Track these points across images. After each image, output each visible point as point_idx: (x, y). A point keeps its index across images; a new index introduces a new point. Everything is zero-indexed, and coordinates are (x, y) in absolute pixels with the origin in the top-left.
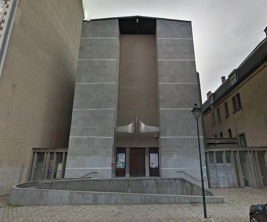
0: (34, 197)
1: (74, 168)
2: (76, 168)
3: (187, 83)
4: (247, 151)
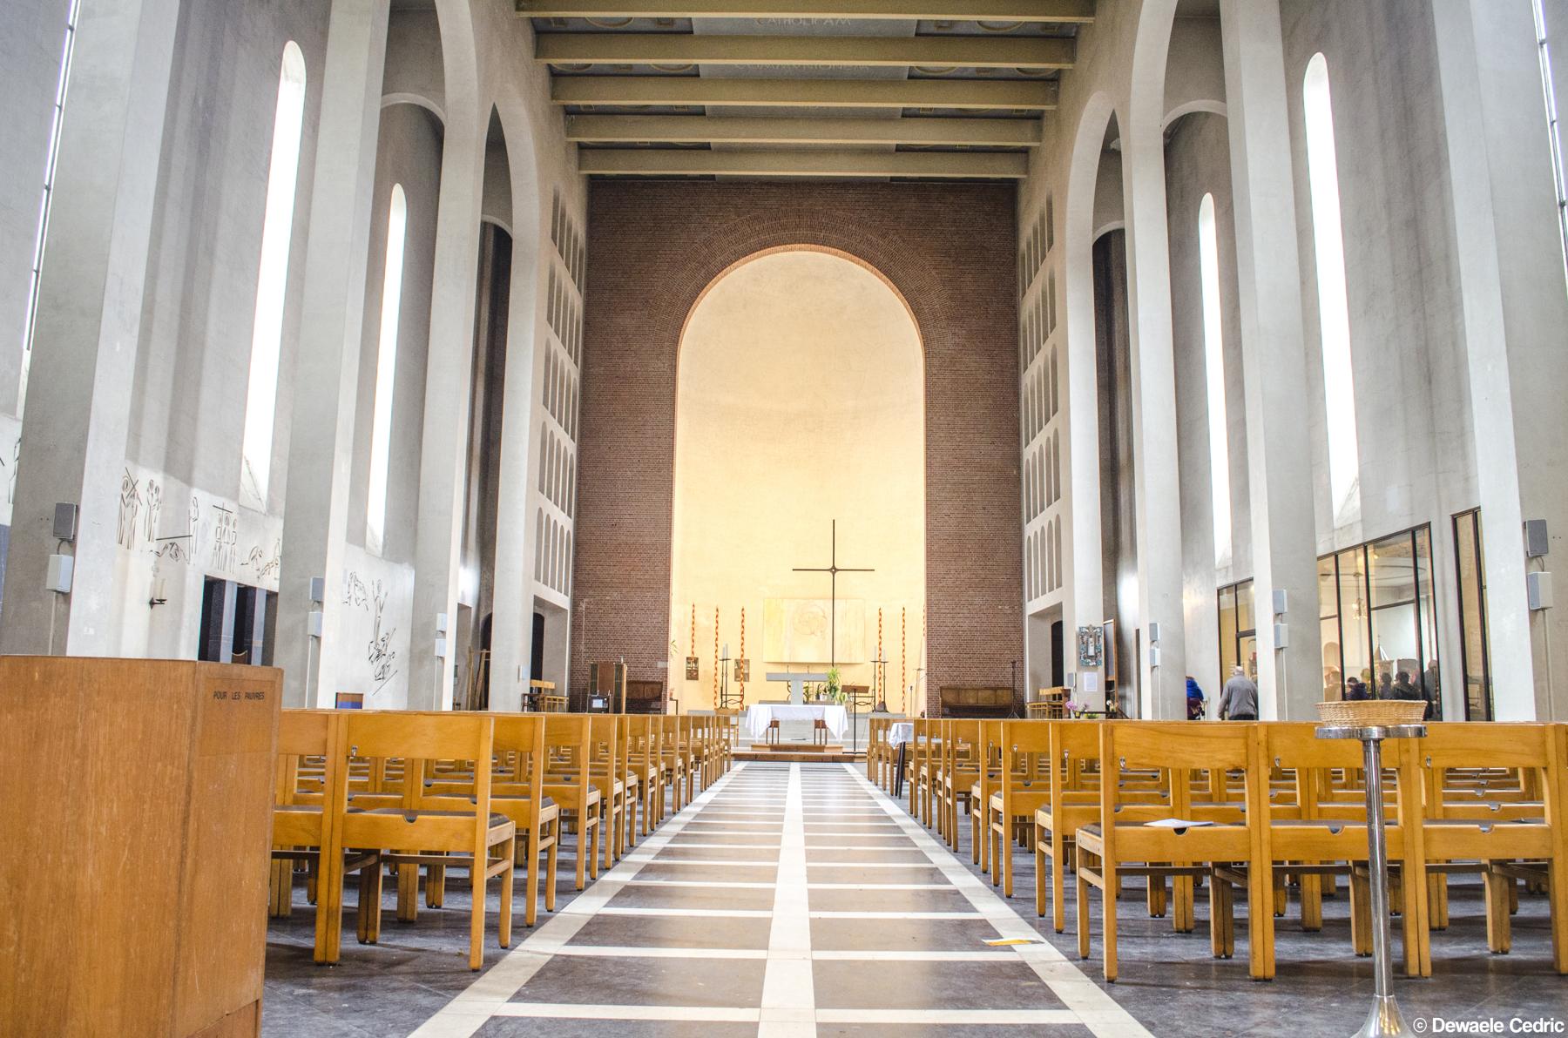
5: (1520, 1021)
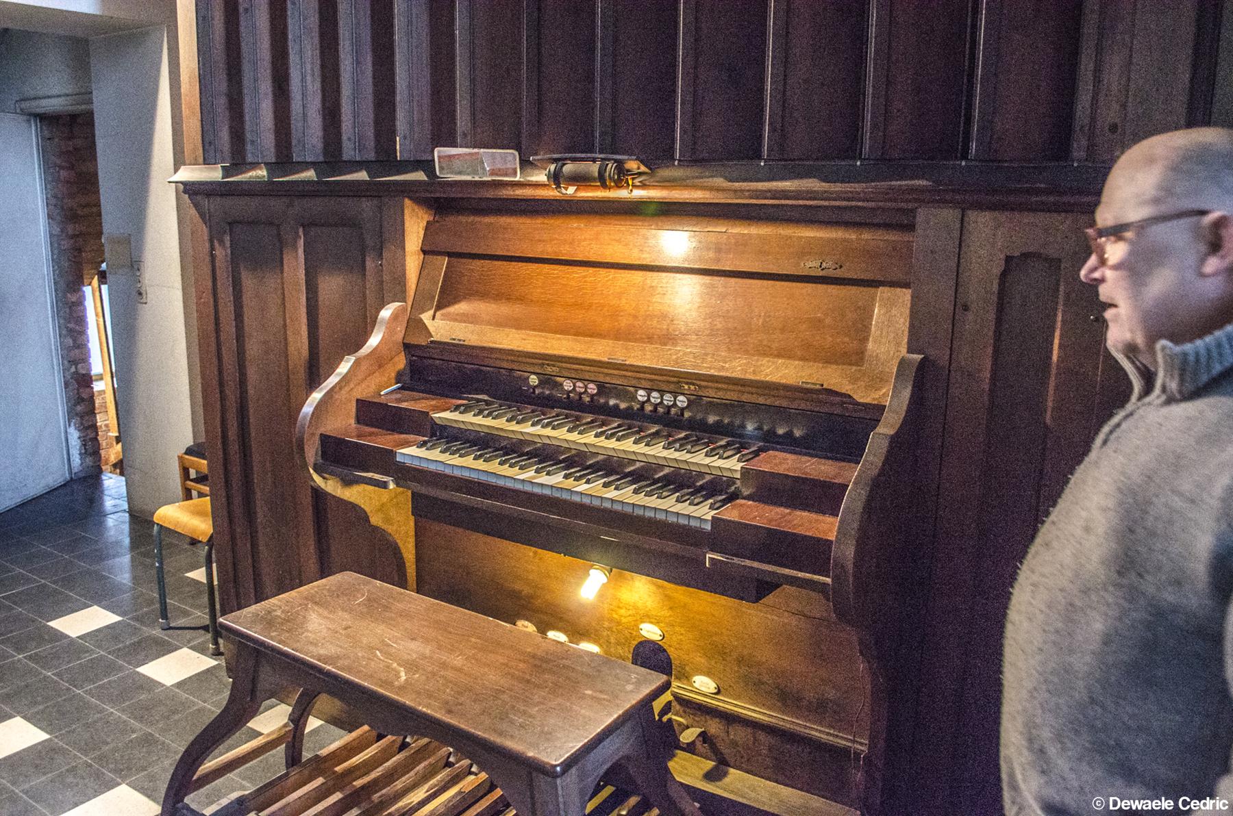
5: (1188, 800)
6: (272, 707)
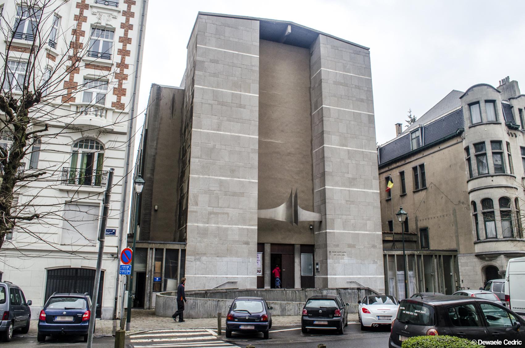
0: (209, 308)
1: (200, 276)
2: (202, 276)
3: (364, 150)
4: (432, 256)
5: (507, 341)
6: (514, 110)
